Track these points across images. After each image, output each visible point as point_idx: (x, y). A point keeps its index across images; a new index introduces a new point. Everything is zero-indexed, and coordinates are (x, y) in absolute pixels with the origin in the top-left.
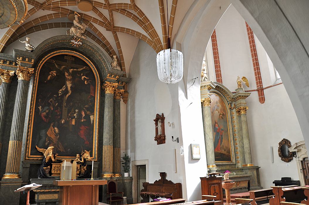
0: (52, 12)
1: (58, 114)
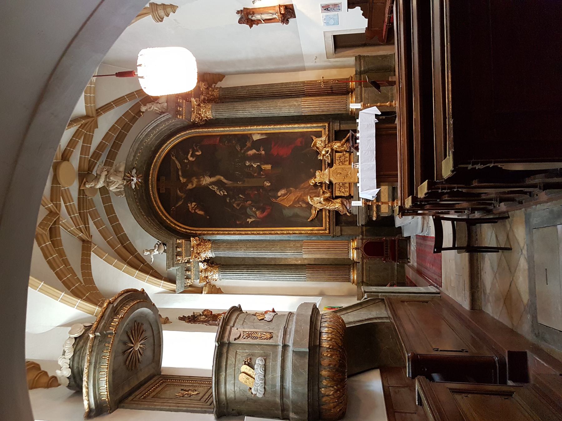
0: (91, 222)
1: (256, 192)
